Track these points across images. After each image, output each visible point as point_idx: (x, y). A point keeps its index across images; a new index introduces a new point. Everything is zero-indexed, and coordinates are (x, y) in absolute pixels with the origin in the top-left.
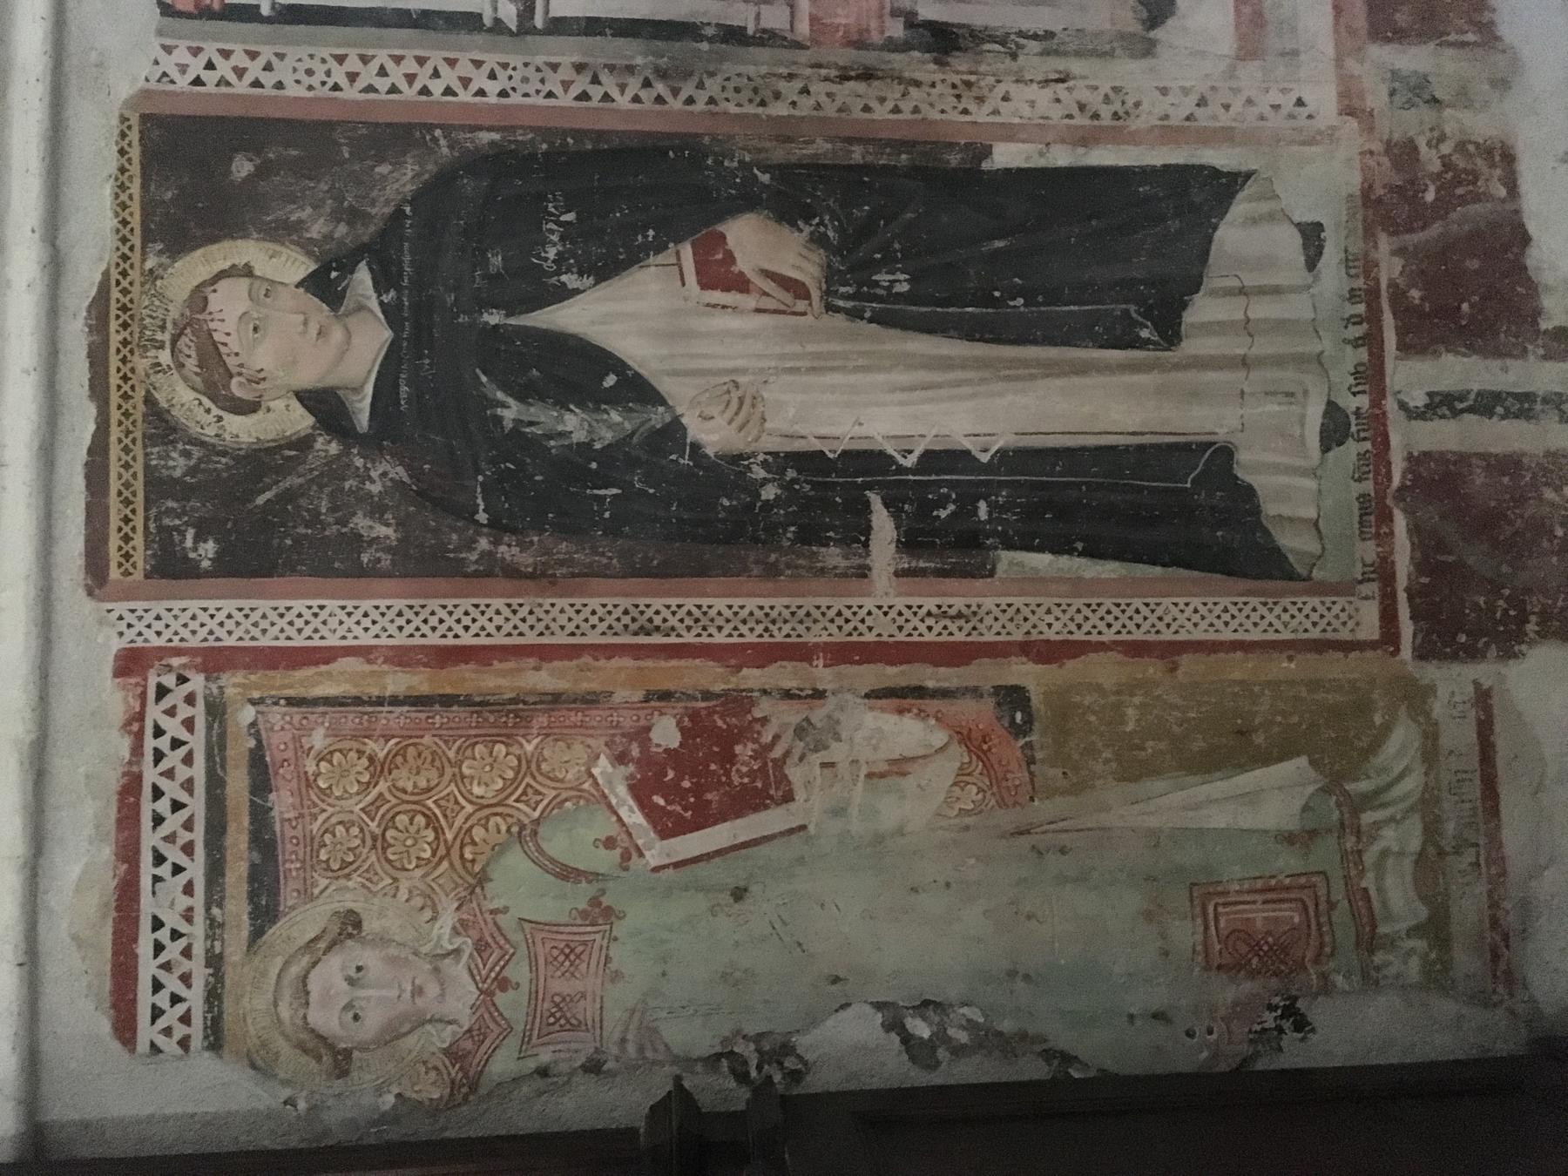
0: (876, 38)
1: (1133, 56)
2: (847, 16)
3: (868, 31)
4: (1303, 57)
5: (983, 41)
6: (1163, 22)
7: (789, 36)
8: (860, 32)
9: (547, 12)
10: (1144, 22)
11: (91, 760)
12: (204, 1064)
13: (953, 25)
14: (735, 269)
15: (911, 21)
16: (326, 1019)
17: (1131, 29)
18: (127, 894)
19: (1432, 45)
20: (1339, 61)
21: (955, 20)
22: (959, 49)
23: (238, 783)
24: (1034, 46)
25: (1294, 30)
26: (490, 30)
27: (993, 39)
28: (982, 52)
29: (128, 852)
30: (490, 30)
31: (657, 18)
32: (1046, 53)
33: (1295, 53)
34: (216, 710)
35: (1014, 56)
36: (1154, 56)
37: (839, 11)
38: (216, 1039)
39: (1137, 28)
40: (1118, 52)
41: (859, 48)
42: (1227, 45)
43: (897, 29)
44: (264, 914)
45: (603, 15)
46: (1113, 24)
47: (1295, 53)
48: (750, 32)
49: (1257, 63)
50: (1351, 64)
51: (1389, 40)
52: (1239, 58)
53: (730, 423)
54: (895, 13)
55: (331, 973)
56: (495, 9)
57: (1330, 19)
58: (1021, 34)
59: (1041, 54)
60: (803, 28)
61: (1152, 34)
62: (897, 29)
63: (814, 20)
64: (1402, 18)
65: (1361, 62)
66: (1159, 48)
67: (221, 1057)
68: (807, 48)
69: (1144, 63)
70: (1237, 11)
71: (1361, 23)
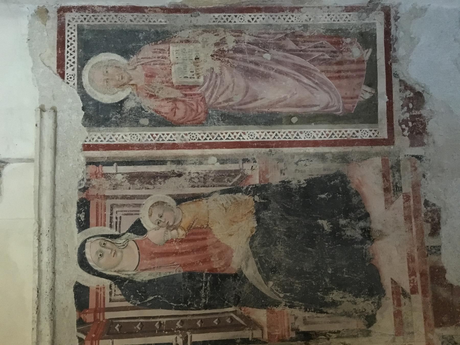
0: (287, 338)
1: (364, 336)
2: (279, 332)
3: (285, 336)
4: (415, 334)
5: (319, 335)
6: (372, 325)
7: (262, 340)
8: (282, 337)
9: (191, 340)
10: (367, 325)
13: (310, 332)
15: (297, 332)
17: (363, 328)
19: (454, 326)
20: (426, 334)
21: (310, 330)
22: (312, 339)
24: (334, 335)
25: (412, 325)
26: (143, 31)
27: (322, 334)
28: (319, 339)
30: (143, 31)
31: (223, 339)
32: (337, 337)
33: (413, 333)
35: (328, 339)
36: (370, 336)
37: (276, 330)
39: (365, 328)
40: (359, 335)
41: (283, 342)
42: (392, 331)
43: (293, 335)
45: (207, 340)
46: (357, 326)
47: (413, 333)
48: (250, 339)
49: (401, 337)
50: (430, 335)
51: (441, 326)
52: (396, 335)
53: (87, 147)
54: (293, 330)
56: (176, 341)
57: (423, 322)
58: (330, 332)
59: (336, 338)
60: (266, 337)
61: (370, 329)
62: (293, 335)
63: (269, 334)
64: (445, 319)
65: (433, 334)
66: (372, 333)
68: (267, 343)
69: (366, 339)
70: (395, 320)
71: (432, 322)
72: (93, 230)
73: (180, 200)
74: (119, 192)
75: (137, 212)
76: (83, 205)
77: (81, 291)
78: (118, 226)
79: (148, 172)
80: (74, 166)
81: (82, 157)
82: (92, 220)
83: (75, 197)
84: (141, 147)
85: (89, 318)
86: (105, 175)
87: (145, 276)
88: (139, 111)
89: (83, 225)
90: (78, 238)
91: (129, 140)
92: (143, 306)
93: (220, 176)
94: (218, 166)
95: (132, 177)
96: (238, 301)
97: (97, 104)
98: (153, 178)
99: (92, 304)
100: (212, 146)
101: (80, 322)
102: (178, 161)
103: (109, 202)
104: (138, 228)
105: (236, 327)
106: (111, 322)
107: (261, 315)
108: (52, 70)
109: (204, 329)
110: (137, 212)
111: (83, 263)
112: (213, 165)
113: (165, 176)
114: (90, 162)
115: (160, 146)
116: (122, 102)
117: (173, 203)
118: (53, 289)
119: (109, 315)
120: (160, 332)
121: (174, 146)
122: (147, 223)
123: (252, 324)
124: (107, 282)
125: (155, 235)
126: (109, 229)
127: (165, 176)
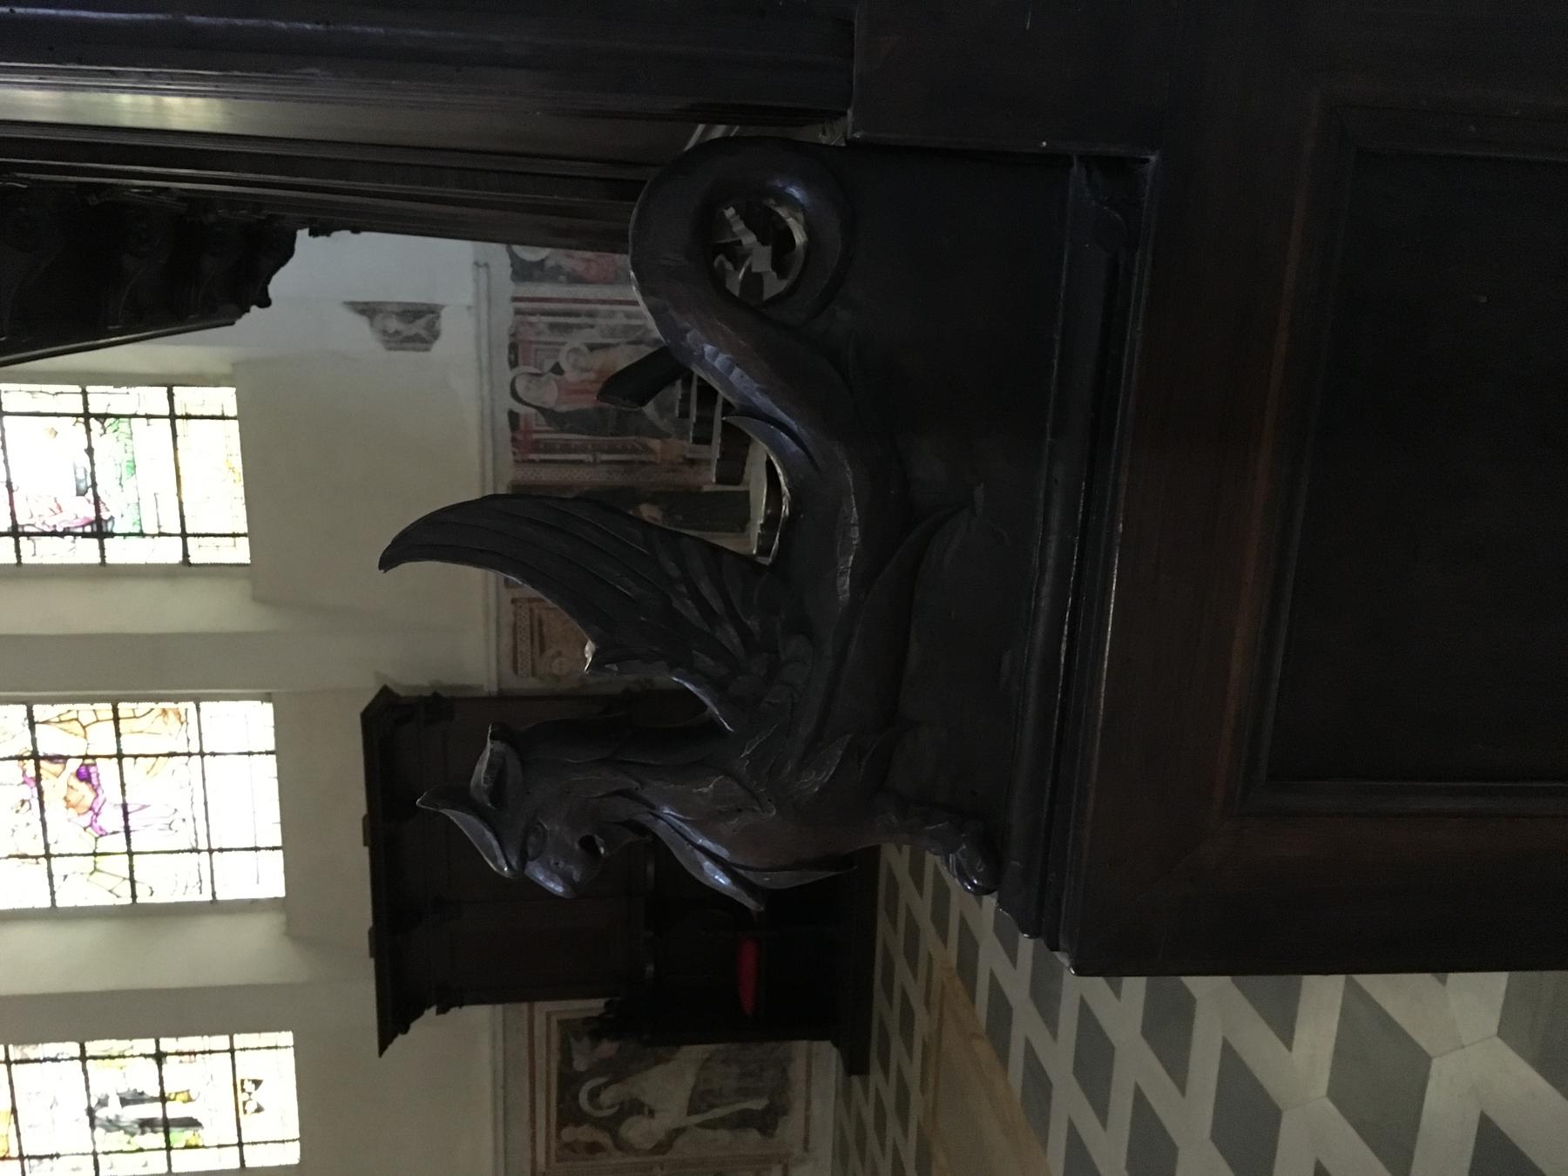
11: (508, 618)
12: (531, 679)
14: (303, 235)
15: (684, 457)
16: (556, 672)
18: (515, 647)
23: (536, 624)
29: (515, 638)
34: (531, 610)
38: (534, 674)
44: (542, 650)
53: (515, 299)
55: (556, 662)
67: (395, 1016)
72: (522, 369)
73: (592, 348)
74: (542, 338)
75: (522, 305)
76: (513, 348)
77: (513, 416)
78: (540, 366)
79: (564, 320)
80: (505, 316)
81: (511, 308)
82: (520, 360)
83: (506, 343)
84: (560, 300)
85: (520, 437)
86: (531, 324)
87: (563, 408)
88: (558, 269)
89: (513, 364)
90: (510, 375)
91: (549, 295)
92: (562, 431)
93: (628, 329)
94: (625, 321)
95: (552, 326)
96: (637, 434)
97: (523, 261)
98: (567, 328)
99: (522, 424)
100: (620, 303)
101: (514, 440)
102: (591, 314)
103: (534, 346)
104: (557, 369)
105: (634, 451)
106: (537, 441)
107: (655, 444)
108: (573, 499)
109: (608, 452)
110: (522, 305)
111: (514, 394)
112: (620, 320)
113: (579, 327)
114: (518, 312)
115: (575, 301)
116: (543, 261)
117: (585, 349)
118: (493, 414)
119: (535, 436)
120: (575, 451)
121: (587, 301)
122: (565, 366)
123: (647, 449)
124: (533, 411)
125: (571, 376)
126: (509, 296)
127: (579, 327)
